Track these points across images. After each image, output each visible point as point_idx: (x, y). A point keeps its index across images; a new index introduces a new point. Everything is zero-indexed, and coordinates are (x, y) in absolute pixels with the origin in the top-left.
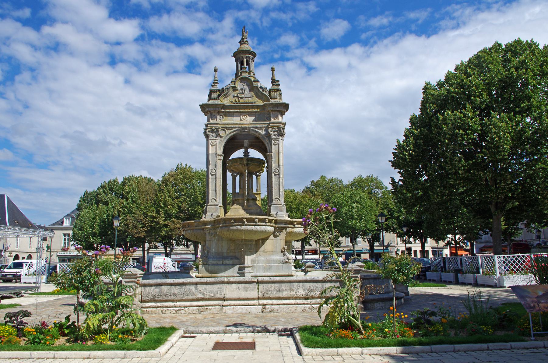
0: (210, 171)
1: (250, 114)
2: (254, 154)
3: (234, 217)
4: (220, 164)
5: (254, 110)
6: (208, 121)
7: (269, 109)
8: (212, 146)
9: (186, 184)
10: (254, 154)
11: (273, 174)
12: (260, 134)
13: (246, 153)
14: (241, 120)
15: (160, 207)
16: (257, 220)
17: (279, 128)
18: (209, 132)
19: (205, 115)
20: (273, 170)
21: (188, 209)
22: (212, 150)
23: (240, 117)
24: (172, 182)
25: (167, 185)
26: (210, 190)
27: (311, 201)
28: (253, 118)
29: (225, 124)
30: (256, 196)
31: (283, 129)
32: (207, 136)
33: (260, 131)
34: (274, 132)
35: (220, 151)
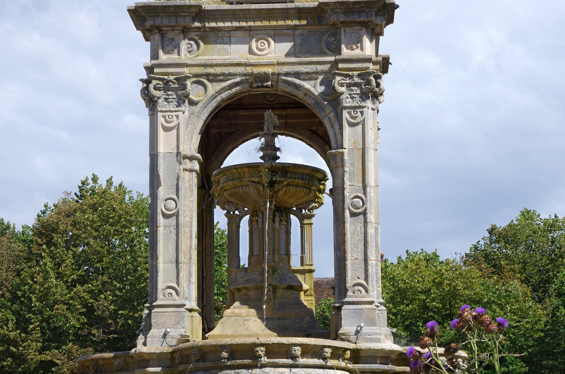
0: (161, 206)
1: (278, 35)
2: (294, 151)
3: (228, 341)
4: (190, 183)
5: (289, 22)
6: (154, 56)
7: (333, 19)
8: (166, 129)
9: (107, 238)
10: (294, 151)
11: (347, 213)
12: (308, 93)
13: (270, 151)
14: (251, 52)
15: (30, 309)
16: (298, 351)
17: (364, 75)
18: (159, 88)
19: (147, 39)
20: (348, 202)
21: (114, 315)
22: (165, 143)
23: (249, 42)
24: (66, 232)
25: (50, 243)
26: (161, 260)
27: (488, 289)
28: (287, 46)
29: (205, 66)
30: (300, 277)
31: (377, 77)
32: (151, 102)
33: (307, 85)
34: (349, 86)
35: (191, 144)
